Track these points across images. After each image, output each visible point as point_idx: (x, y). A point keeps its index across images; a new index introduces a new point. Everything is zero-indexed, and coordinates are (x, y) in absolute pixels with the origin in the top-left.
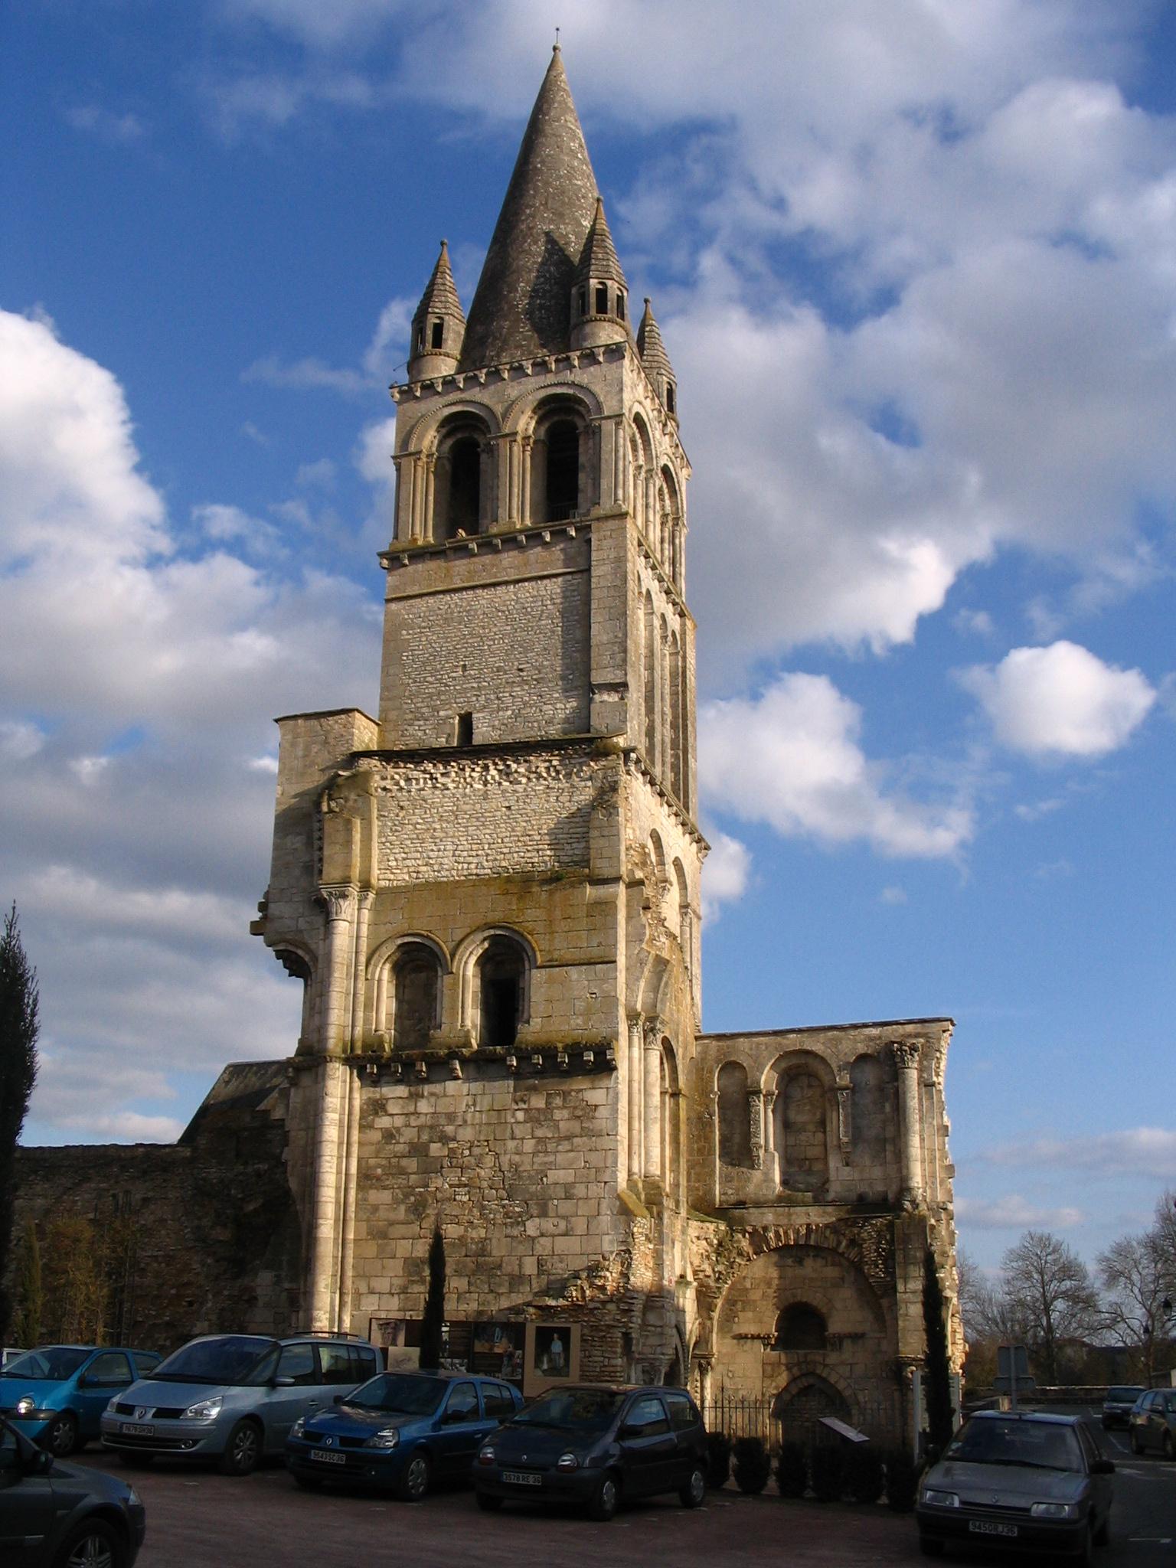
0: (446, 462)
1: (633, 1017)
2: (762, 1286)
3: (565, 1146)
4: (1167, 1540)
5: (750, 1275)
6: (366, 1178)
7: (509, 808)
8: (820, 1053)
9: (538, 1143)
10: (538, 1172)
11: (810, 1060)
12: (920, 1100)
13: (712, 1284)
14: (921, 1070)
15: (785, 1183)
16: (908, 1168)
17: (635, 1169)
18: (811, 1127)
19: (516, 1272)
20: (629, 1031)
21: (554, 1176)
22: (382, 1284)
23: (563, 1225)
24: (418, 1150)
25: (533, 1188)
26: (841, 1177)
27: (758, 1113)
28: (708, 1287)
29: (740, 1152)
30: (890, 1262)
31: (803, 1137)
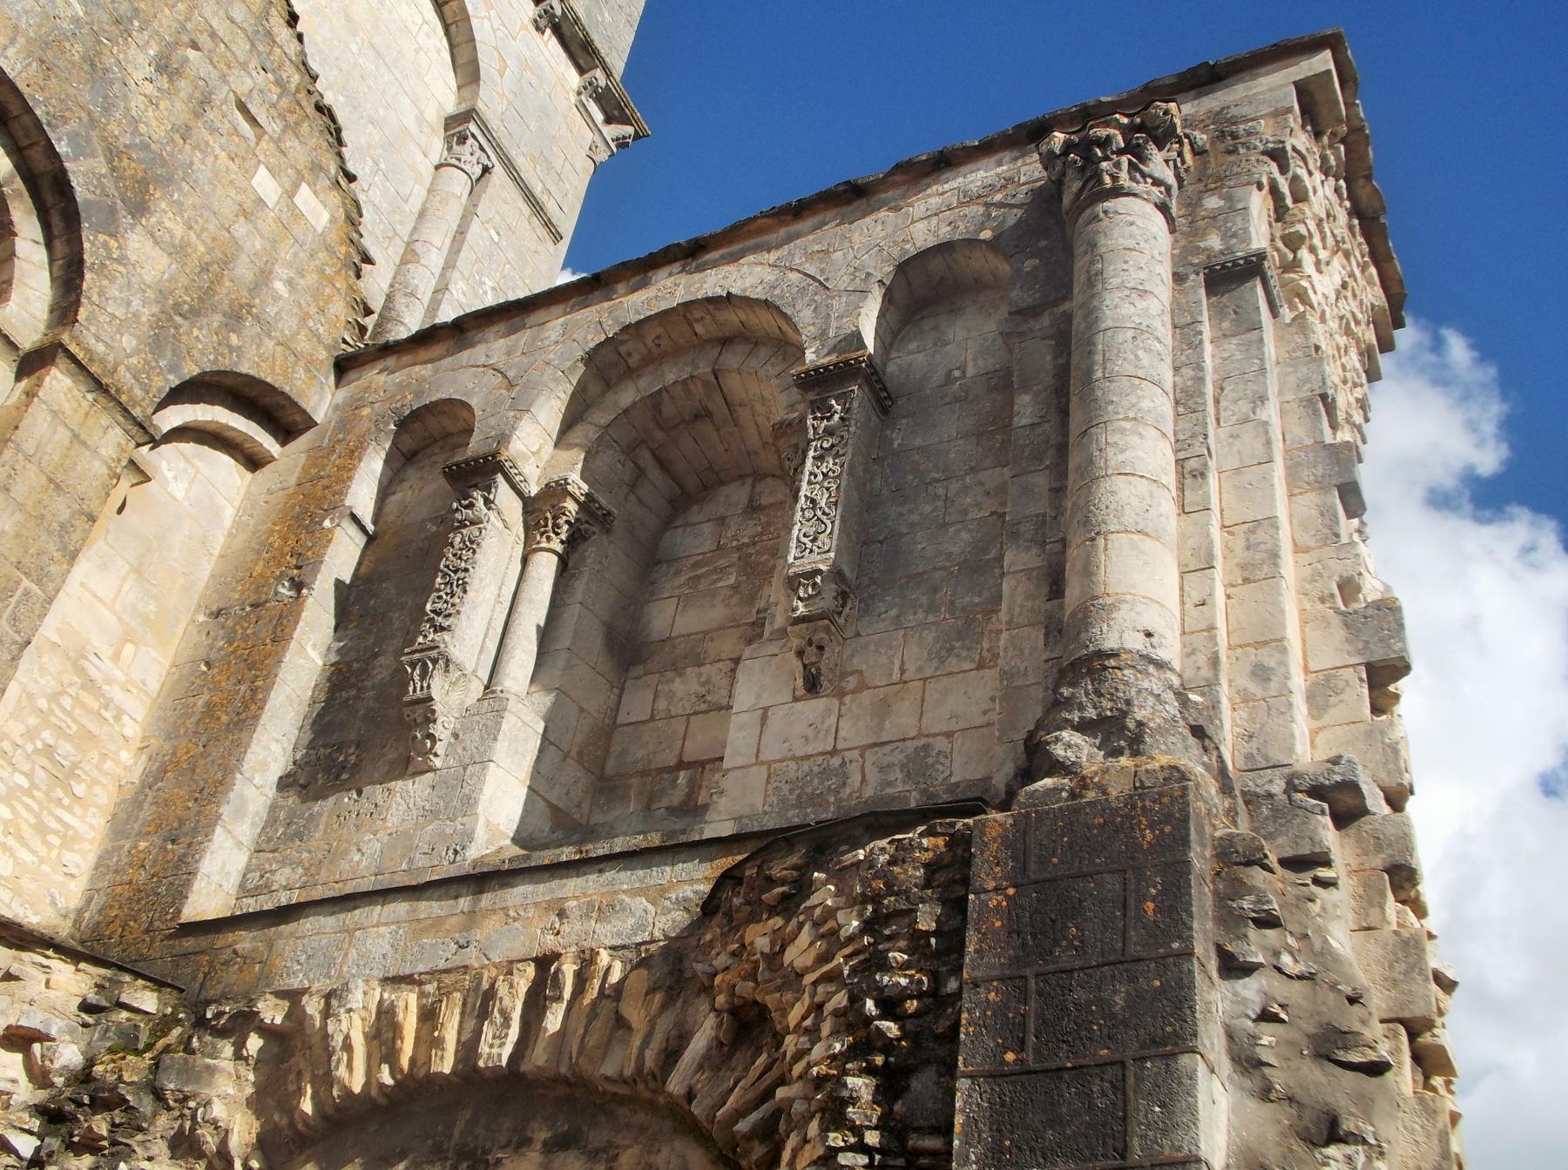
8: (758, 293)
11: (732, 359)
12: (1185, 331)
14: (1184, 220)
16: (1088, 571)
26: (767, 739)
29: (370, 726)
30: (922, 1083)
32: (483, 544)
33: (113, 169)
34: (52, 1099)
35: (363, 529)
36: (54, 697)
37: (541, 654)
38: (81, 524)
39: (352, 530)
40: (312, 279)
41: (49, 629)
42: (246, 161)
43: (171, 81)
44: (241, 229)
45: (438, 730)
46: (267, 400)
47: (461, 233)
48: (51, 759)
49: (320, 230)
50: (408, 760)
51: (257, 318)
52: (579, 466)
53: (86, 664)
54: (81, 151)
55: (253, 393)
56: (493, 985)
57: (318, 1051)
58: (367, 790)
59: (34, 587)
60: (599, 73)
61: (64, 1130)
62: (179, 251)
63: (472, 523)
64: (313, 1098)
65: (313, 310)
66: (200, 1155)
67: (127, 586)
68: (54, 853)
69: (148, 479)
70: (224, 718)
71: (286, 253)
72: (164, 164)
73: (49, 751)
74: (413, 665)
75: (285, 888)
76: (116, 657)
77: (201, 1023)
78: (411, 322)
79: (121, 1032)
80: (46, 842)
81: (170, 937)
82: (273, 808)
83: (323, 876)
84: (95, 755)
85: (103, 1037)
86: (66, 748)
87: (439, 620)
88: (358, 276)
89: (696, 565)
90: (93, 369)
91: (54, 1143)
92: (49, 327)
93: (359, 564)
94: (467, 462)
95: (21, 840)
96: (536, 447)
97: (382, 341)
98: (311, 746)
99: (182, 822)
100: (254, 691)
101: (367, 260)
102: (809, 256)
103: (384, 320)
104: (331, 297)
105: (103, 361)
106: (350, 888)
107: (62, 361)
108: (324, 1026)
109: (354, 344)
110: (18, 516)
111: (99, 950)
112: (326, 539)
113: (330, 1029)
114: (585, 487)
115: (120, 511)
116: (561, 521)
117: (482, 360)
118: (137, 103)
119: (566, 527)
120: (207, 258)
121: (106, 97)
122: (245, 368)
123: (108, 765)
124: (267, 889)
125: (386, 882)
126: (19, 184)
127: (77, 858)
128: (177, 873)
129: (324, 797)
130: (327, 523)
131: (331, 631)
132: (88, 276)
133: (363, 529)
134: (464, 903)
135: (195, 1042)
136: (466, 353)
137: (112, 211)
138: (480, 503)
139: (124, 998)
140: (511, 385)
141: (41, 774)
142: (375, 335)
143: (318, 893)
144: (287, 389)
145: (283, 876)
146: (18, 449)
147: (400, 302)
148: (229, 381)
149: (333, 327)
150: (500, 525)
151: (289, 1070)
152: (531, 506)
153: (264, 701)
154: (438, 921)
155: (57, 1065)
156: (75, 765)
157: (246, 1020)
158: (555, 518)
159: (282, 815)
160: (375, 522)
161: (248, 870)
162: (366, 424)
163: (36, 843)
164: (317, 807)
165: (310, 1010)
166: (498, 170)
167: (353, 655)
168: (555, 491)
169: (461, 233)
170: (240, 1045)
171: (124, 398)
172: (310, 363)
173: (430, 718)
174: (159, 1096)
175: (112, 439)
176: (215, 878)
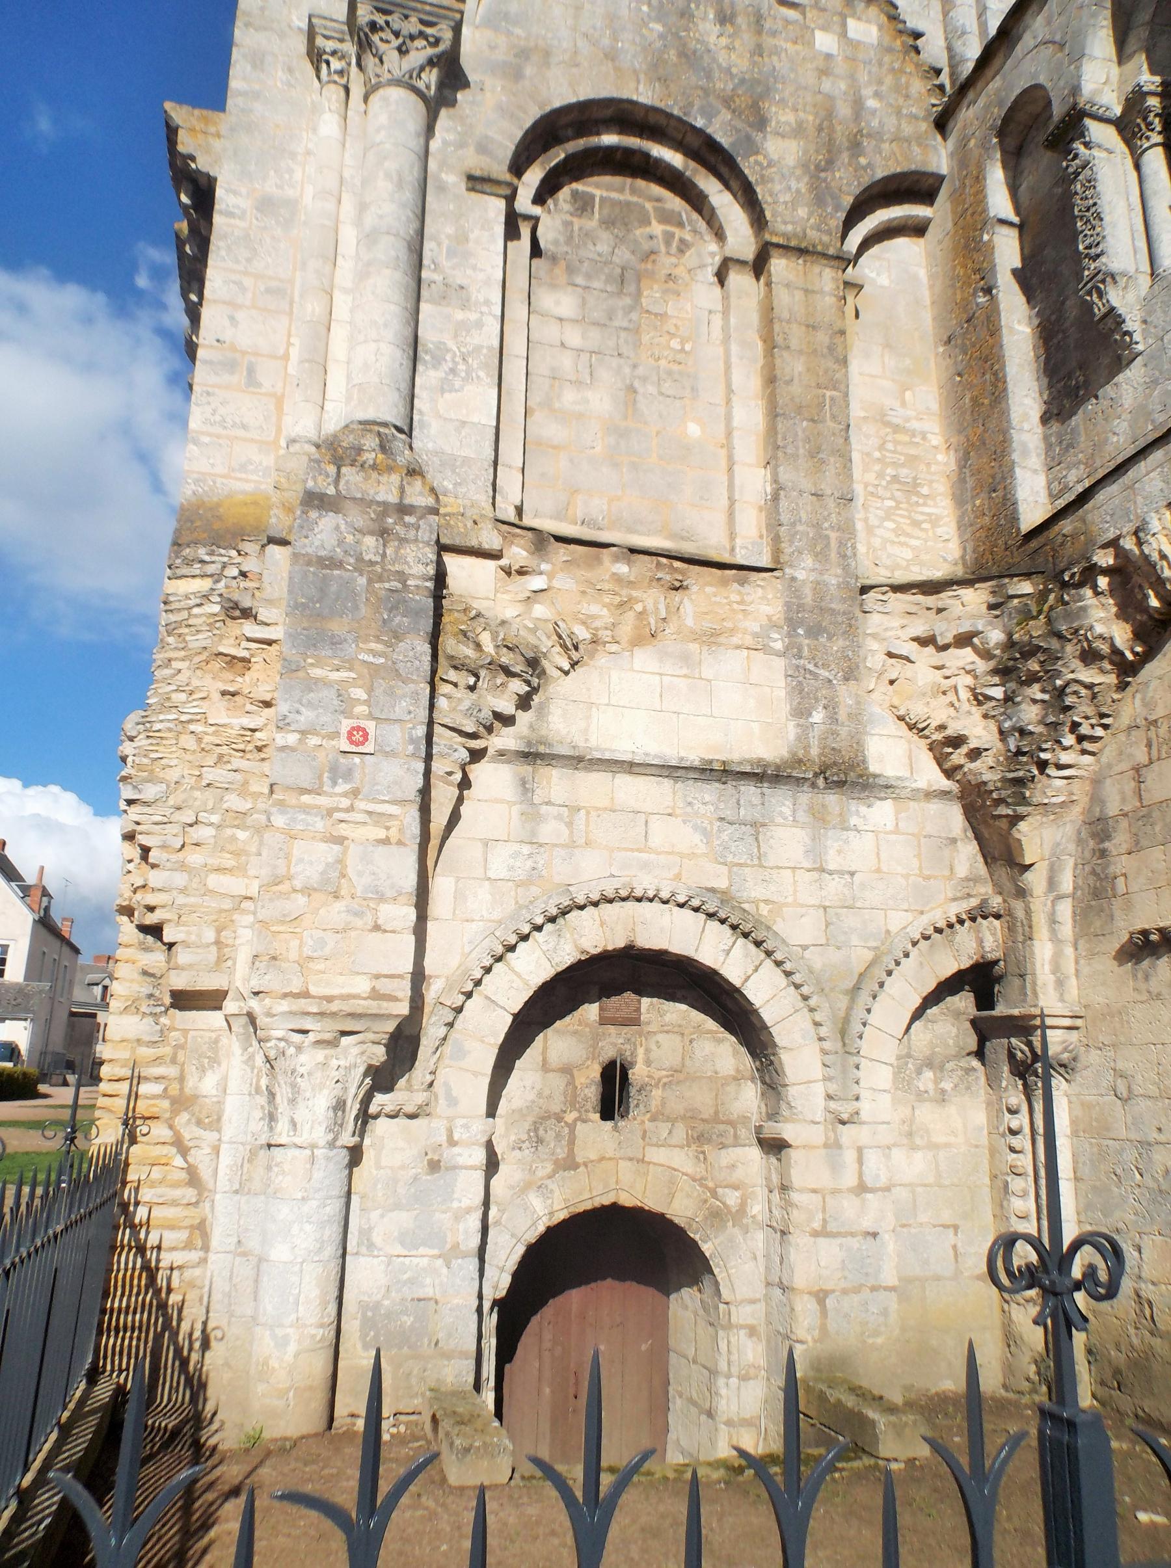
5: (1042, 722)
32: (1099, 177)
33: (734, 111)
34: (999, 663)
35: (1011, 224)
36: (882, 447)
38: (838, 340)
39: (1005, 230)
40: (889, 80)
41: (856, 411)
42: (804, 37)
43: (732, 24)
44: (827, 85)
45: (1129, 326)
46: (906, 184)
48: (899, 482)
49: (876, 42)
50: (1119, 358)
51: (869, 136)
52: (1145, 66)
53: (888, 418)
54: (710, 116)
55: (893, 187)
57: (1146, 568)
58: (1100, 393)
59: (834, 393)
61: (1014, 676)
62: (798, 131)
63: (1084, 167)
64: (1156, 596)
65: (901, 101)
66: (1102, 658)
67: (886, 359)
68: (930, 533)
69: (862, 287)
70: (986, 402)
71: (863, 77)
72: (758, 82)
73: (895, 479)
74: (1089, 293)
75: (1078, 482)
76: (903, 404)
77: (1065, 585)
78: (973, 51)
79: (1019, 611)
80: (922, 530)
81: (1021, 545)
82: (1046, 438)
83: (1098, 463)
84: (922, 467)
85: (1010, 618)
86: (904, 472)
87: (1093, 251)
88: (918, 52)
90: (793, 244)
92: (756, 237)
93: (1022, 249)
94: (1057, 127)
95: (908, 535)
97: (958, 84)
98: (1050, 386)
99: (993, 477)
100: (995, 374)
101: (918, 35)
103: (953, 67)
104: (907, 83)
105: (795, 235)
106: (1119, 460)
107: (774, 252)
108: (1142, 552)
109: (937, 102)
110: (803, 359)
111: (984, 573)
112: (989, 248)
113: (1147, 551)
114: (1158, 79)
115: (857, 316)
116: (1150, 119)
117: (1032, 43)
118: (722, 58)
119: (1157, 120)
120: (818, 122)
121: (704, 69)
122: (880, 174)
123: (933, 468)
125: (1141, 444)
126: (692, 164)
127: (945, 529)
128: (1007, 507)
129: (1075, 413)
130: (986, 237)
131: (1026, 306)
132: (758, 189)
133: (1011, 224)
135: (1066, 597)
136: (1019, 48)
137: (748, 138)
138: (1082, 149)
139: (1011, 592)
140: (1062, 46)
141: (898, 494)
142: (953, 82)
143: (1099, 475)
144: (913, 167)
145: (1073, 476)
146: (780, 320)
147: (958, 45)
148: (875, 190)
149: (922, 100)
150: (1104, 155)
151: (1133, 587)
153: (1005, 376)
155: (992, 644)
156: (915, 479)
157: (1090, 573)
158: (1145, 119)
159: (1053, 439)
160: (1018, 213)
161: (1049, 484)
162: (976, 153)
163: (916, 532)
164: (1074, 421)
165: (1127, 547)
167: (1048, 312)
168: (1135, 99)
170: (1095, 587)
171: (819, 248)
172: (920, 139)
173: (1119, 321)
174: (1059, 636)
175: (827, 277)
176: (1031, 499)
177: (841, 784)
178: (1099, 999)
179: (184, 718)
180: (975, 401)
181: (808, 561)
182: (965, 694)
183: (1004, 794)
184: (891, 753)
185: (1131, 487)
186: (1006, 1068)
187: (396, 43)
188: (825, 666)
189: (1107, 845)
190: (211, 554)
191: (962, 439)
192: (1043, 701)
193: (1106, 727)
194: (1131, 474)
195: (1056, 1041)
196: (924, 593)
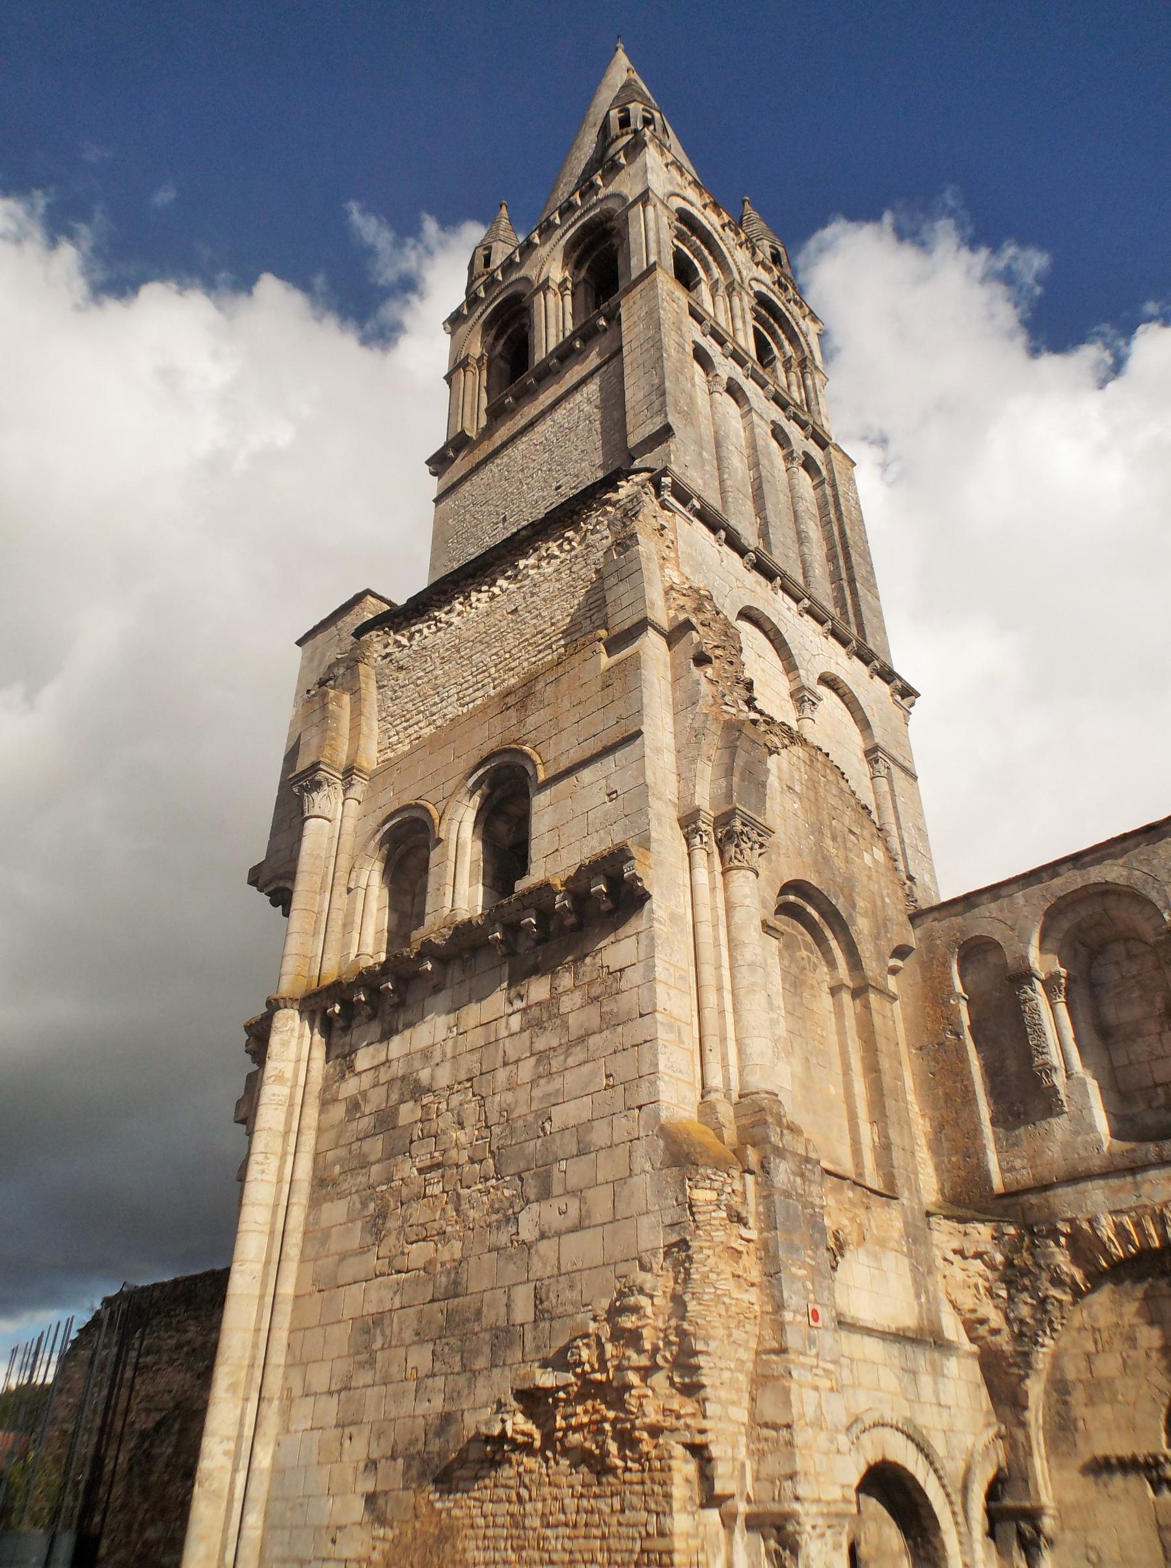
0: (502, 364)
1: (689, 823)
2: (1118, 1344)
3: (578, 1054)
4: (1104, 1264)
5: (1033, 1317)
6: (323, 1185)
7: (515, 611)
9: (538, 1062)
10: (538, 1114)
13: (1008, 1348)
15: (1115, 1134)
17: (716, 1080)
18: (1152, 1026)
19: (502, 1323)
20: (688, 845)
21: (562, 1115)
22: (320, 1378)
23: (574, 1207)
24: (386, 1120)
25: (530, 1147)
27: (1036, 1011)
28: (998, 1354)
29: (1024, 1095)
31: (1140, 1048)
37: (1078, 1048)
47: (895, 807)
56: (1162, 1211)
58: (1038, 1123)
60: (898, 682)
89: (1116, 987)
91: (1013, 1291)
96: (1041, 961)
98: (995, 1103)
102: (1140, 861)
124: (1012, 1169)
134: (1129, 1179)
152: (1043, 983)
154: (1121, 1188)
166: (892, 766)
169: (895, 807)
177: (941, 1346)
178: (1070, 1497)
179: (719, 1292)
180: (948, 1096)
181: (906, 1194)
182: (982, 1291)
183: (1018, 1360)
184: (952, 1328)
185: (1083, 1192)
186: (1015, 1543)
187: (750, 844)
188: (921, 1265)
189: (1068, 1398)
190: (715, 1174)
191: (937, 1114)
192: (1032, 1305)
193: (1062, 1325)
194: (1082, 1186)
195: (1048, 1524)
196: (959, 1222)
